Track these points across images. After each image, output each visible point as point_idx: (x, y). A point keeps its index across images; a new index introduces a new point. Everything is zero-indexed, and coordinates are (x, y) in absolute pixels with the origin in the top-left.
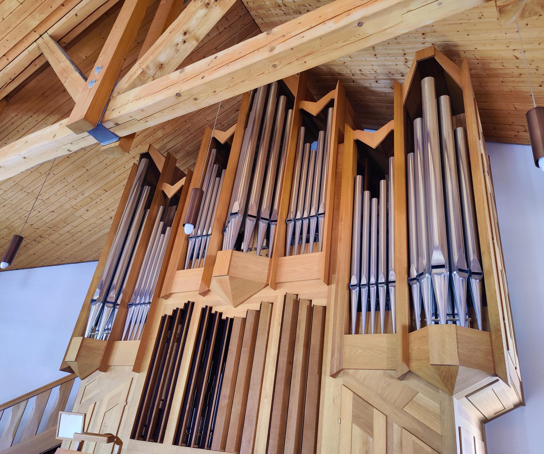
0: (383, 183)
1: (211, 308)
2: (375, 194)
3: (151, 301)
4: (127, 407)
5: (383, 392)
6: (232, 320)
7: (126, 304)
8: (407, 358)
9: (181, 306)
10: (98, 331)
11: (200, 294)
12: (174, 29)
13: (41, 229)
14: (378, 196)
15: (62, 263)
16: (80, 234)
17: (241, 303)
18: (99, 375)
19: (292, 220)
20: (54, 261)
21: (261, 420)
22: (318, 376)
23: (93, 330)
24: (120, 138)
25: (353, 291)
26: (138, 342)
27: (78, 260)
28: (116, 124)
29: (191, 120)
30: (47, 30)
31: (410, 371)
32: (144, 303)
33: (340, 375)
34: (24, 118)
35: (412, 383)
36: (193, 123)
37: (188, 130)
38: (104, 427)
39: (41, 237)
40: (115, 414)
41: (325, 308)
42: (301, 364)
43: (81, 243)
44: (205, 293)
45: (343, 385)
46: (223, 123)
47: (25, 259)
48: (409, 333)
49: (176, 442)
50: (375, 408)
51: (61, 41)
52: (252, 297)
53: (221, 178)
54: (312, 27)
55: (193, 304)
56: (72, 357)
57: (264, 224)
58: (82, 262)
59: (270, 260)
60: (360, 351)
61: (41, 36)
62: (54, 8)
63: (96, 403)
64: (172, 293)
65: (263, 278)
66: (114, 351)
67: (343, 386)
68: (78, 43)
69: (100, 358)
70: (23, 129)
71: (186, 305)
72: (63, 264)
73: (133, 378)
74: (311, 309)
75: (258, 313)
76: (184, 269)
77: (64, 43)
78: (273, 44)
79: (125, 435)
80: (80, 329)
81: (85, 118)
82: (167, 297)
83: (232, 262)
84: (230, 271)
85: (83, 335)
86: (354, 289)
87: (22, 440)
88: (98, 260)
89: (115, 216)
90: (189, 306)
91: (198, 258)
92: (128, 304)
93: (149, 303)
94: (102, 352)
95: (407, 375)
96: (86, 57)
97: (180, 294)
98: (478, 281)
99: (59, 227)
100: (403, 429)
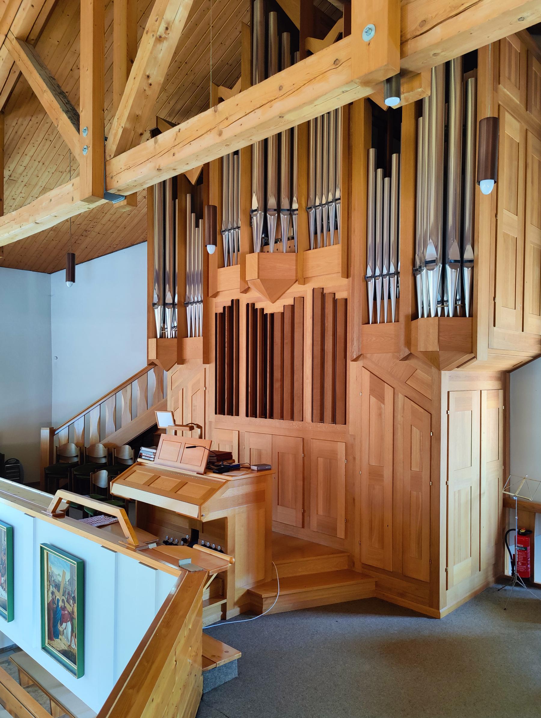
0: (394, 156)
1: (253, 305)
2: (387, 174)
5: (392, 370)
7: (183, 304)
8: (408, 343)
9: (229, 304)
10: (167, 328)
11: (242, 292)
12: (137, 74)
13: (83, 224)
14: (390, 176)
15: (114, 250)
16: (120, 220)
17: (278, 299)
18: (177, 367)
19: (312, 208)
20: (107, 249)
21: (306, 397)
22: (344, 360)
23: (163, 329)
24: (126, 196)
25: (369, 282)
27: (129, 244)
28: (118, 190)
29: (191, 71)
30: (9, 27)
31: (411, 353)
32: (198, 302)
33: (360, 359)
34: (25, 123)
35: (412, 362)
36: (195, 75)
37: (193, 83)
38: (194, 406)
39: (86, 231)
41: (346, 300)
42: (331, 351)
43: (125, 228)
44: (246, 291)
45: (363, 367)
46: (230, 62)
47: (80, 254)
48: (412, 321)
50: (386, 383)
51: (28, 39)
52: (286, 292)
53: (238, 155)
54: (246, 113)
55: (238, 301)
56: (153, 356)
57: (286, 216)
58: (133, 245)
59: (296, 255)
60: (374, 339)
61: (6, 36)
63: (183, 389)
64: (219, 292)
65: (292, 275)
66: (184, 347)
67: (363, 368)
68: (45, 30)
69: (176, 353)
70: (28, 135)
72: (116, 251)
73: (205, 368)
74: (335, 301)
75: (293, 307)
76: (224, 267)
77: (33, 40)
78: (221, 126)
81: (92, 195)
82: (216, 295)
83: (260, 265)
84: (260, 274)
85: (156, 337)
86: (370, 281)
87: (138, 415)
88: (146, 241)
89: (147, 204)
90: (236, 303)
91: (234, 252)
92: (184, 304)
93: (202, 301)
94: (176, 349)
96: (58, 41)
98: (470, 269)
99: (98, 218)
100: (405, 397)
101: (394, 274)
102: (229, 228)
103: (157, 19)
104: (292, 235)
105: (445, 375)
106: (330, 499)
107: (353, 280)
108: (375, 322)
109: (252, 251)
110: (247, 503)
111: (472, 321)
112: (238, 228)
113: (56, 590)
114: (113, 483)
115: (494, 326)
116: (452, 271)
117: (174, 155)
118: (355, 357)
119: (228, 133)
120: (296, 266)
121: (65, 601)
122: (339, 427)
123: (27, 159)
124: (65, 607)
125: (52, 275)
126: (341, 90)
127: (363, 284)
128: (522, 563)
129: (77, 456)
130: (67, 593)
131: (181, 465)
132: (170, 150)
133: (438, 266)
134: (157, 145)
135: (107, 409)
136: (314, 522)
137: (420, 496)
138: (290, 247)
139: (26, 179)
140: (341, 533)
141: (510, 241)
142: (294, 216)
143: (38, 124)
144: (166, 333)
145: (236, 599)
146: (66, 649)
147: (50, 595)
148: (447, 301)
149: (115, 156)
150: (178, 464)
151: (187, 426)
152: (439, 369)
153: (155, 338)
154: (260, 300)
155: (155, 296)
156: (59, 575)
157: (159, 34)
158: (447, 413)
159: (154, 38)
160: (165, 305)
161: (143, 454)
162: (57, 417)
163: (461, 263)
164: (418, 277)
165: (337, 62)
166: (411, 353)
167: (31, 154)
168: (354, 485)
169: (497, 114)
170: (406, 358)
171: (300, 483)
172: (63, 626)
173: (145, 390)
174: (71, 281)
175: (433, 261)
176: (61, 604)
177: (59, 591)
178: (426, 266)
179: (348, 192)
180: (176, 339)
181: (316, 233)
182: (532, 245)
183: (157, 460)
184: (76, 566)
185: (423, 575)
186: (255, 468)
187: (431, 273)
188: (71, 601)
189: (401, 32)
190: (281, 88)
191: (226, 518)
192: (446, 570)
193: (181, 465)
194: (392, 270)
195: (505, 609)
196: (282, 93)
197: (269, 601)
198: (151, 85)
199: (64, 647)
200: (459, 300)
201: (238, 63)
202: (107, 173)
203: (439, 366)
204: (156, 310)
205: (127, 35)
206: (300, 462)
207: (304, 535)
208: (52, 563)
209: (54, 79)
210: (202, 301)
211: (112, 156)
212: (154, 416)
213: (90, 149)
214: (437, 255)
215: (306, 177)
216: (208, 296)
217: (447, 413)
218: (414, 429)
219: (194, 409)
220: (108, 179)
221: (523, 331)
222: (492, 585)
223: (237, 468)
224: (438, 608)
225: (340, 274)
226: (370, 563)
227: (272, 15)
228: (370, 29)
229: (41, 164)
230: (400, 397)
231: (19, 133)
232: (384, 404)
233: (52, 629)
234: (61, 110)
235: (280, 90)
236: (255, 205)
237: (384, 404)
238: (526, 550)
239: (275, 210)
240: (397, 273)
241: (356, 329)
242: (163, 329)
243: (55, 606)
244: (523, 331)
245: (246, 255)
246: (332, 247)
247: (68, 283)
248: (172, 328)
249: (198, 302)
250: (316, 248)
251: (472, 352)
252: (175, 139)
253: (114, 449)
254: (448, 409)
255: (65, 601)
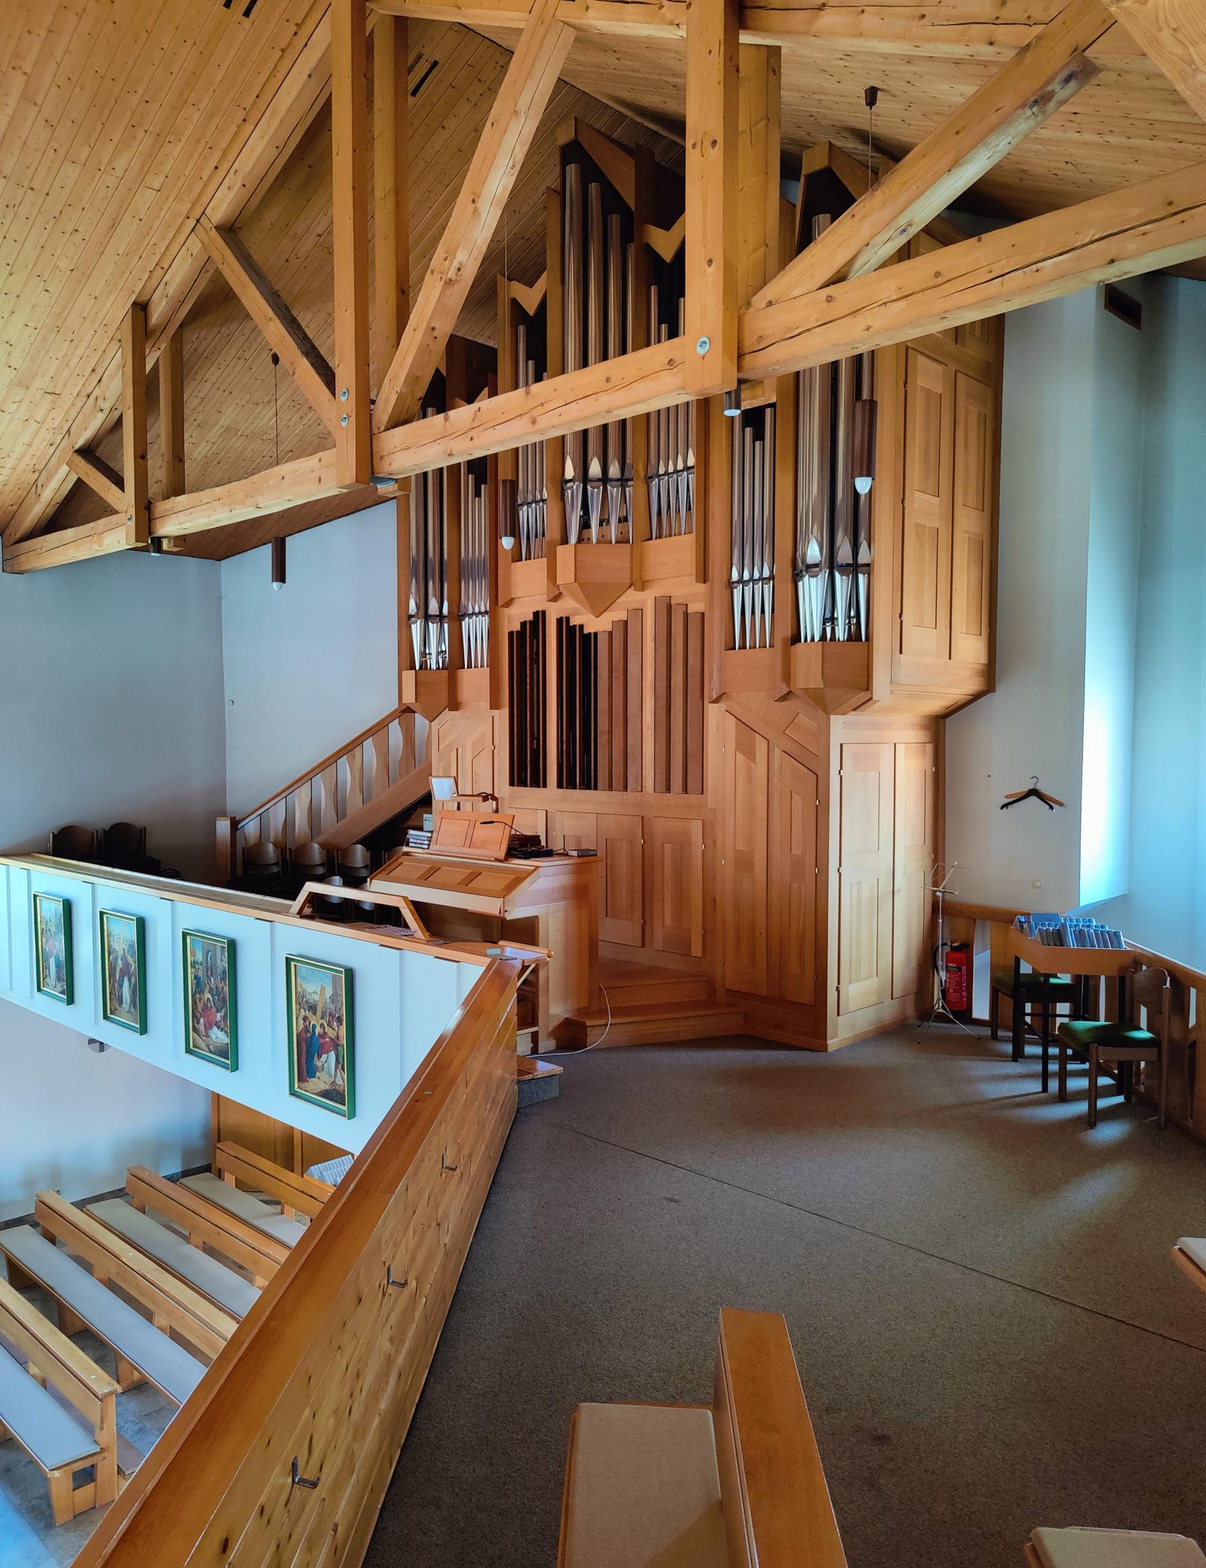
1: (568, 619)
3: (488, 609)
4: (496, 751)
6: (596, 634)
7: (456, 616)
9: (531, 617)
17: (604, 612)
18: (448, 715)
23: (424, 654)
24: (397, 480)
26: (487, 670)
31: (790, 691)
32: (480, 613)
38: (476, 775)
40: (484, 760)
44: (556, 598)
46: (526, 236)
49: (560, 786)
55: (544, 612)
56: (409, 697)
61: (198, 221)
62: (205, 178)
64: (513, 599)
66: (459, 683)
69: (446, 693)
71: (536, 614)
76: (521, 560)
78: (534, 413)
79: (503, 788)
80: (408, 664)
81: (357, 481)
82: (509, 603)
90: (539, 617)
91: (536, 537)
92: (458, 616)
93: (486, 612)
94: (445, 686)
95: (986, 662)
97: (526, 598)
101: (769, 579)
102: (530, 500)
103: (447, 257)
104: (625, 514)
105: (837, 722)
106: (681, 899)
107: (712, 588)
108: (743, 647)
109: (565, 540)
110: (563, 899)
111: (868, 645)
112: (543, 501)
113: (311, 1014)
114: (371, 880)
115: (901, 653)
116: (842, 580)
117: (472, 439)
118: (715, 697)
119: (542, 422)
120: (631, 562)
121: (325, 1024)
122: (692, 798)
123: (207, 386)
124: (325, 1033)
125: (222, 561)
126: (676, 393)
127: (727, 592)
128: (954, 989)
129: (276, 864)
130: (328, 1013)
131: (472, 851)
132: (468, 432)
133: (823, 571)
134: (447, 423)
135: (322, 785)
136: (659, 937)
137: (803, 889)
138: (621, 533)
139: (201, 417)
140: (697, 950)
141: (927, 533)
142: (627, 489)
143: (229, 338)
144: (428, 661)
145: (550, 1029)
146: (328, 1088)
147: (301, 1021)
148: (837, 619)
149: (387, 429)
150: (466, 850)
151: (479, 795)
152: (828, 713)
153: (411, 669)
154: (577, 613)
155: (412, 604)
156: (315, 992)
157: (449, 276)
158: (840, 773)
159: (443, 281)
160: (427, 618)
161: (411, 840)
162: (236, 801)
163: (853, 569)
164: (800, 584)
165: (672, 362)
166: (790, 691)
167: (213, 379)
168: (714, 879)
169: (909, 355)
170: (784, 698)
171: (639, 882)
172: (321, 1059)
173: (383, 751)
174: (281, 581)
175: (816, 565)
176: (318, 1030)
177: (315, 1013)
178: (807, 572)
179: (705, 459)
180: (445, 673)
181: (659, 513)
182: (967, 536)
183: (434, 847)
184: (343, 976)
185: (806, 997)
186: (575, 853)
187: (813, 580)
188: (335, 1023)
189: (738, 343)
190: (608, 380)
191: (537, 917)
192: (838, 989)
193: (472, 851)
194: (766, 574)
195: (919, 1043)
196: (609, 385)
197: (596, 1031)
198: (436, 338)
199: (324, 1087)
200: (854, 617)
201: (542, 237)
202: (374, 452)
203: (826, 709)
204: (413, 626)
205: (397, 257)
206: (639, 853)
207: (644, 958)
208: (303, 978)
209: (279, 296)
210: (486, 612)
211: (382, 429)
212: (428, 784)
213: (353, 418)
214: (822, 556)
215: (644, 434)
216: (497, 604)
217: (840, 773)
218: (795, 796)
219: (476, 780)
220: (375, 459)
221: (950, 658)
222: (913, 1021)
223: (549, 853)
224: (825, 1039)
225: (694, 577)
226: (737, 987)
227: (593, 187)
228: (705, 342)
229: (227, 393)
230: (777, 752)
231: (200, 350)
232: (755, 763)
233: (305, 1066)
234: (298, 352)
235: (607, 381)
236: (570, 472)
237: (755, 763)
238: (960, 969)
239: (599, 480)
240: (772, 577)
241: (716, 656)
242: (424, 654)
243: (309, 1035)
244: (950, 658)
245: (558, 547)
246: (683, 537)
247: (276, 585)
248: (438, 654)
249: (480, 613)
250: (659, 537)
251: (868, 689)
252: (474, 420)
253: (338, 850)
254: (841, 769)
255: (325, 1024)
